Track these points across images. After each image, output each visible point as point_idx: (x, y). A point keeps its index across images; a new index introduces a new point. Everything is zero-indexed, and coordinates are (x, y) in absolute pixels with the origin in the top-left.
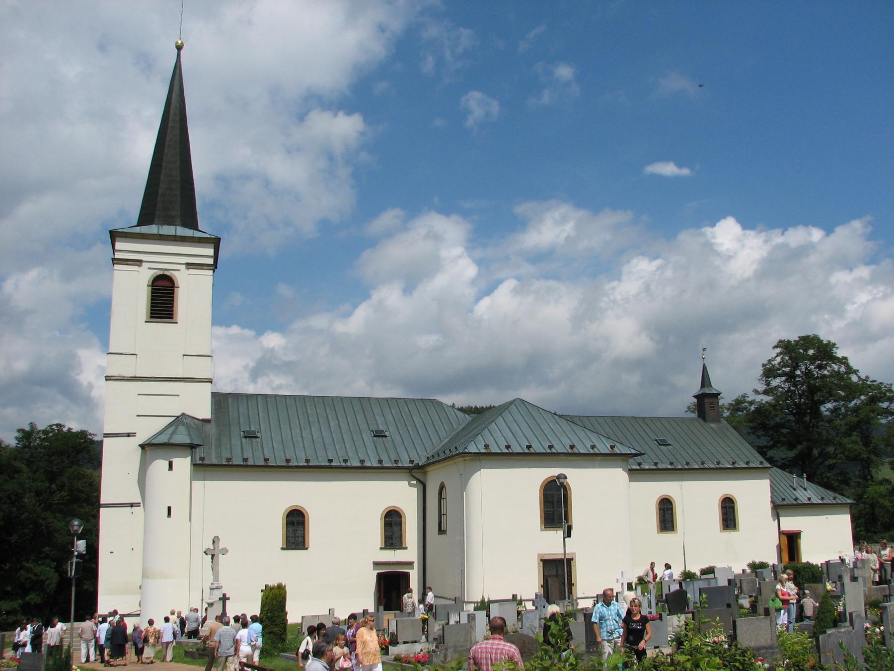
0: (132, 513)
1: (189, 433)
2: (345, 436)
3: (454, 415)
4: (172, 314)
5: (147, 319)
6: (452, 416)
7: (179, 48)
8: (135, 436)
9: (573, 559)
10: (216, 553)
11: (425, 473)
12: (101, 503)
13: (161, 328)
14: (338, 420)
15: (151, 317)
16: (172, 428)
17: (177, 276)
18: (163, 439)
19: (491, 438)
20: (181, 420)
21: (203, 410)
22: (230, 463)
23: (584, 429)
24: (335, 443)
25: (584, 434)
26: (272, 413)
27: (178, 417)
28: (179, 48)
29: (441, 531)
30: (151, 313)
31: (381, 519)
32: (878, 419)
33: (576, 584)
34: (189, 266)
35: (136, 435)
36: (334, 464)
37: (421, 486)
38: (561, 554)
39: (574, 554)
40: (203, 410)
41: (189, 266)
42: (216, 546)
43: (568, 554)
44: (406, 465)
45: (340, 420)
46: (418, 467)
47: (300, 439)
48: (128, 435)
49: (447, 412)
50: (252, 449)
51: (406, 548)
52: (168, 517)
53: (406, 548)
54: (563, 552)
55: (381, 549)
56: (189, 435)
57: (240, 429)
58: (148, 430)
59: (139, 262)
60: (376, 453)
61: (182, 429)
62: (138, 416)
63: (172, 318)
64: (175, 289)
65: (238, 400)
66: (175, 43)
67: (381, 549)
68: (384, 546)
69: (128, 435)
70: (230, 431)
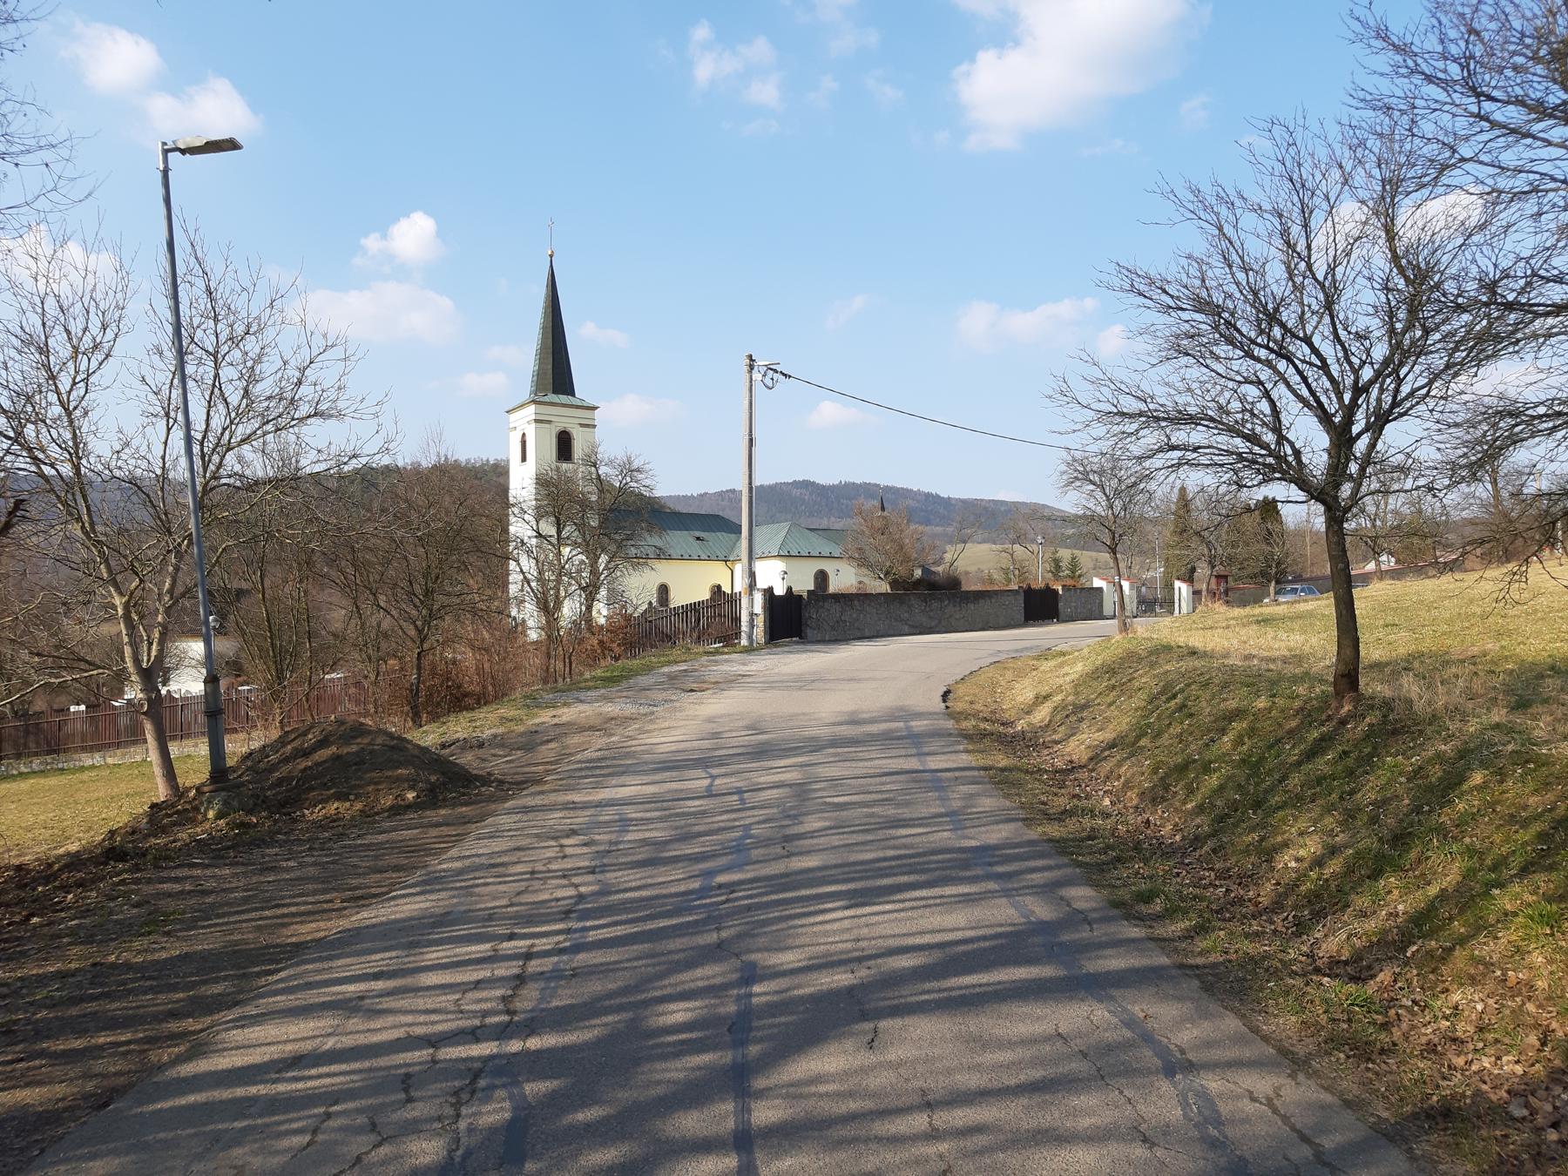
41: (582, 425)
59: (549, 422)
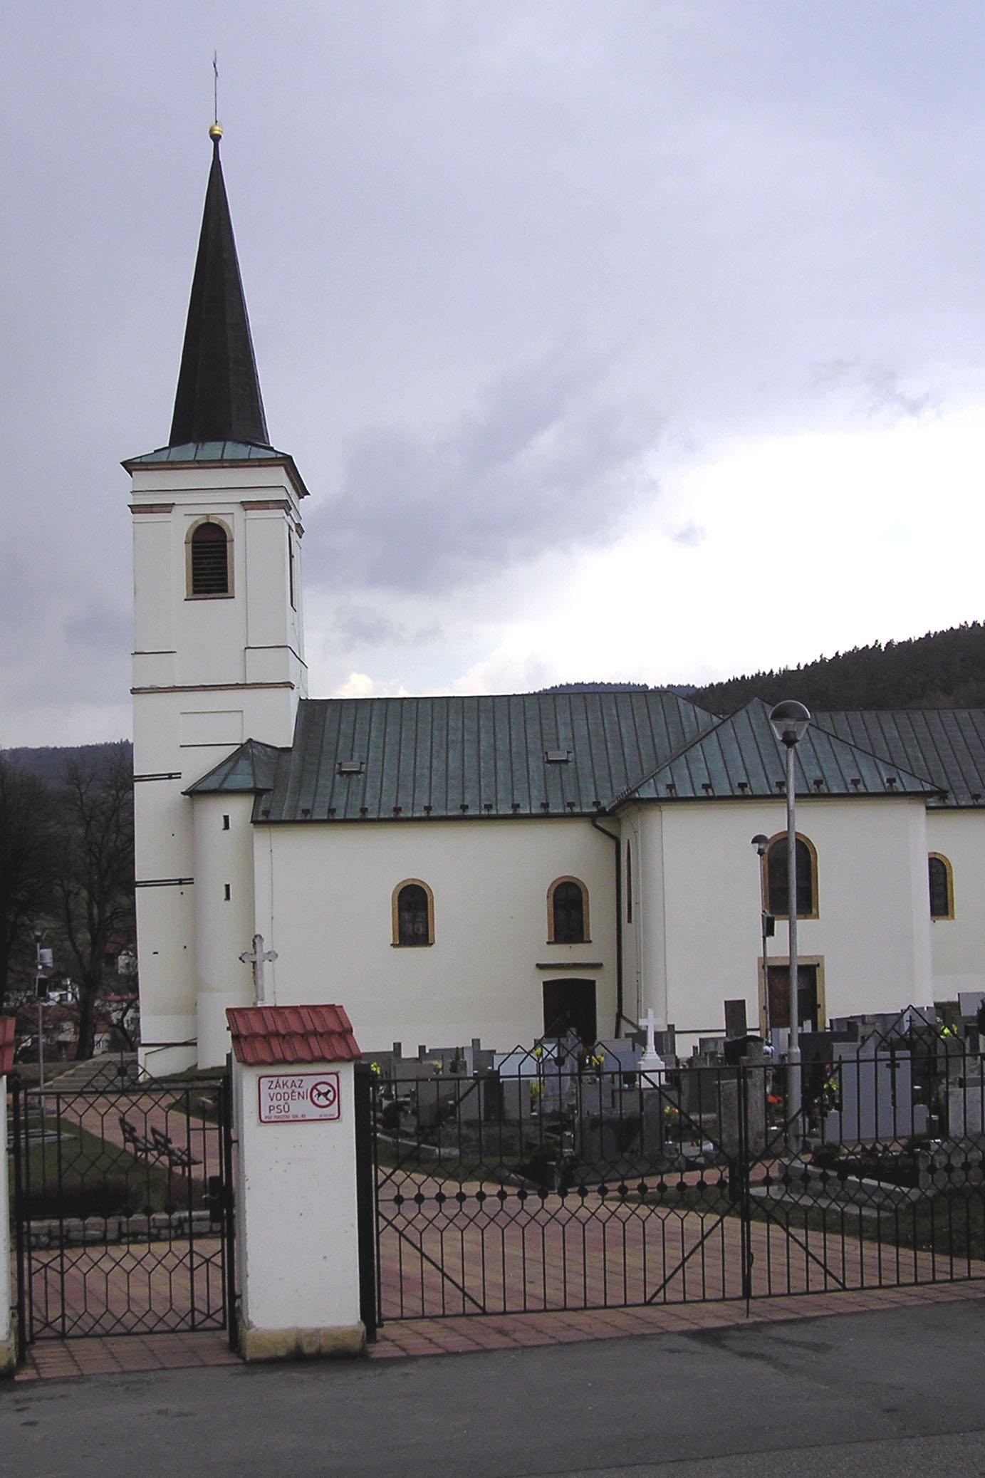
0: (182, 893)
1: (254, 772)
2: (499, 764)
3: (693, 719)
4: (226, 585)
5: (187, 595)
6: (688, 718)
7: (216, 138)
8: (180, 778)
9: (818, 965)
10: (258, 958)
11: (618, 821)
12: (137, 880)
13: (211, 607)
14: (495, 736)
15: (195, 592)
16: (230, 764)
17: (226, 520)
18: (213, 784)
19: (686, 772)
20: (248, 751)
21: (281, 733)
22: (308, 817)
23: (855, 750)
24: (482, 775)
25: (850, 758)
26: (392, 729)
27: (242, 745)
28: (216, 138)
29: (629, 921)
30: (195, 586)
31: (548, 897)
32: (45, 966)
33: (824, 1005)
34: (247, 505)
35: (182, 776)
36: (470, 812)
37: (612, 843)
38: (785, 958)
39: (822, 957)
40: (281, 733)
41: (247, 505)
42: (258, 949)
43: (770, 958)
44: (586, 810)
45: (499, 736)
46: (602, 813)
47: (426, 772)
48: (170, 776)
49: (682, 711)
50: (348, 791)
51: (590, 942)
52: (226, 900)
53: (590, 942)
54: (788, 954)
55: (548, 943)
56: (254, 774)
57: (336, 759)
58: (196, 767)
59: (168, 508)
60: (543, 793)
61: (244, 765)
62: (181, 746)
63: (226, 591)
64: (228, 544)
65: (341, 709)
66: (208, 130)
67: (548, 943)
68: (553, 940)
69: (170, 776)
70: (320, 762)
